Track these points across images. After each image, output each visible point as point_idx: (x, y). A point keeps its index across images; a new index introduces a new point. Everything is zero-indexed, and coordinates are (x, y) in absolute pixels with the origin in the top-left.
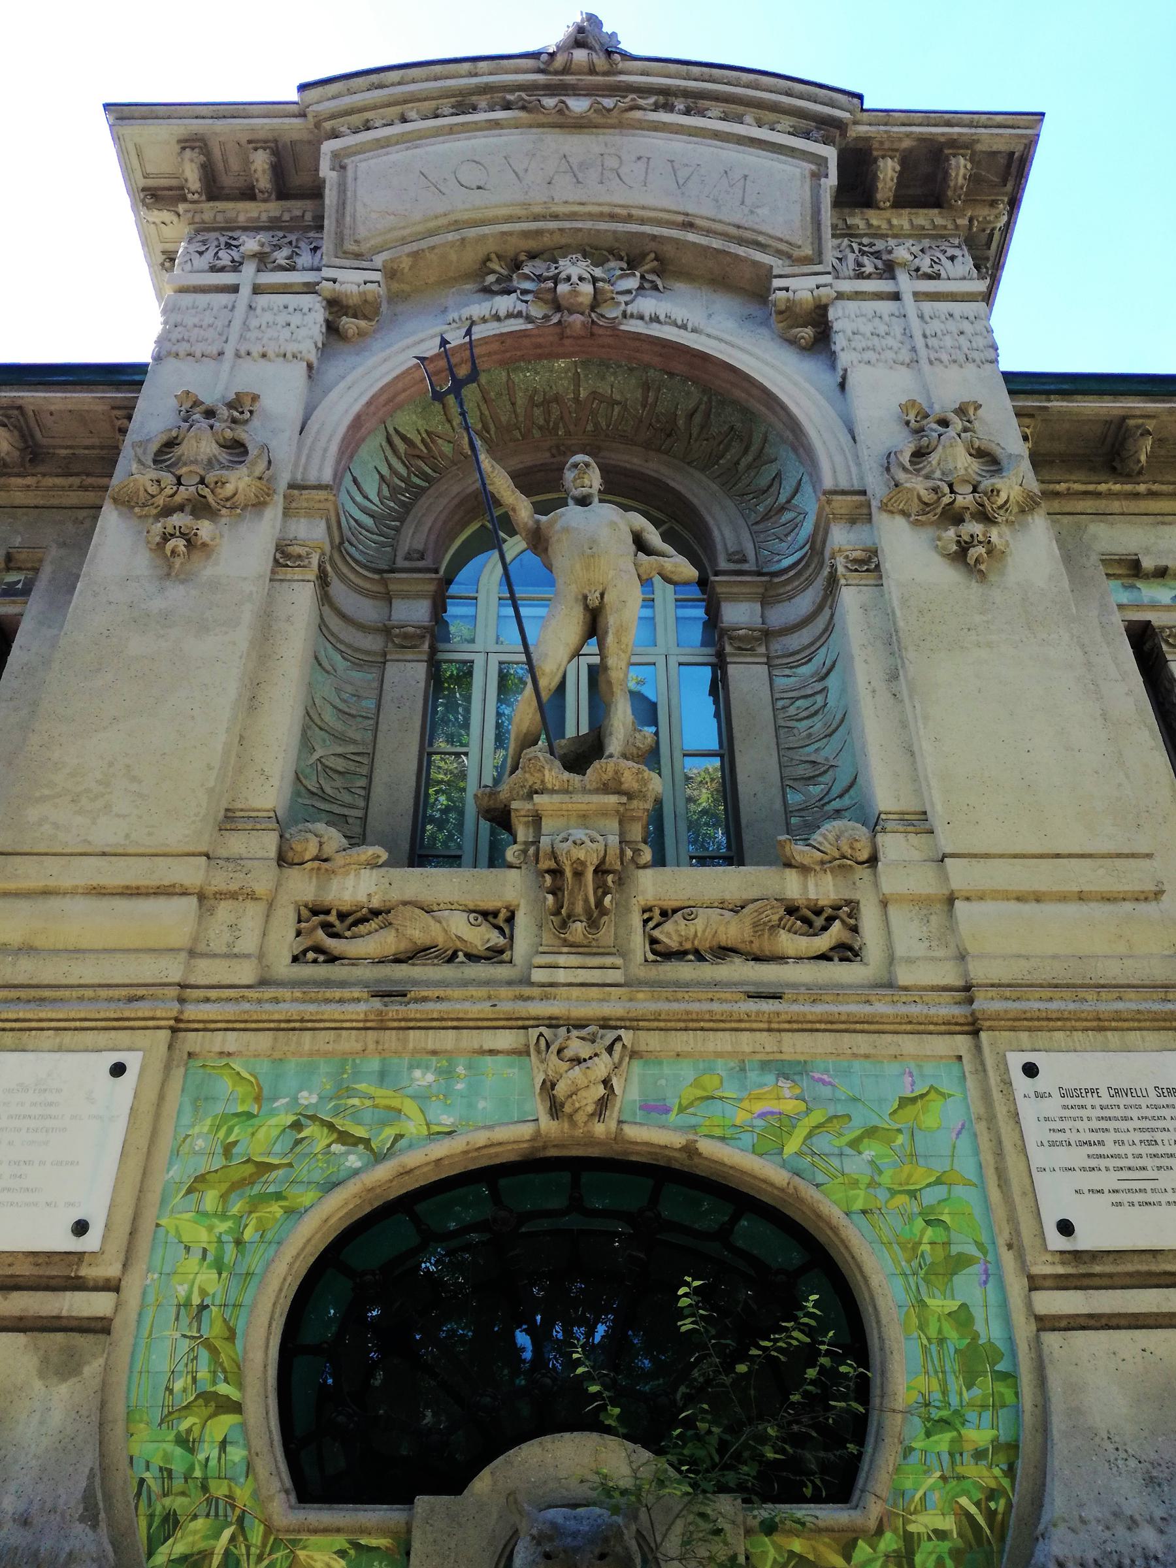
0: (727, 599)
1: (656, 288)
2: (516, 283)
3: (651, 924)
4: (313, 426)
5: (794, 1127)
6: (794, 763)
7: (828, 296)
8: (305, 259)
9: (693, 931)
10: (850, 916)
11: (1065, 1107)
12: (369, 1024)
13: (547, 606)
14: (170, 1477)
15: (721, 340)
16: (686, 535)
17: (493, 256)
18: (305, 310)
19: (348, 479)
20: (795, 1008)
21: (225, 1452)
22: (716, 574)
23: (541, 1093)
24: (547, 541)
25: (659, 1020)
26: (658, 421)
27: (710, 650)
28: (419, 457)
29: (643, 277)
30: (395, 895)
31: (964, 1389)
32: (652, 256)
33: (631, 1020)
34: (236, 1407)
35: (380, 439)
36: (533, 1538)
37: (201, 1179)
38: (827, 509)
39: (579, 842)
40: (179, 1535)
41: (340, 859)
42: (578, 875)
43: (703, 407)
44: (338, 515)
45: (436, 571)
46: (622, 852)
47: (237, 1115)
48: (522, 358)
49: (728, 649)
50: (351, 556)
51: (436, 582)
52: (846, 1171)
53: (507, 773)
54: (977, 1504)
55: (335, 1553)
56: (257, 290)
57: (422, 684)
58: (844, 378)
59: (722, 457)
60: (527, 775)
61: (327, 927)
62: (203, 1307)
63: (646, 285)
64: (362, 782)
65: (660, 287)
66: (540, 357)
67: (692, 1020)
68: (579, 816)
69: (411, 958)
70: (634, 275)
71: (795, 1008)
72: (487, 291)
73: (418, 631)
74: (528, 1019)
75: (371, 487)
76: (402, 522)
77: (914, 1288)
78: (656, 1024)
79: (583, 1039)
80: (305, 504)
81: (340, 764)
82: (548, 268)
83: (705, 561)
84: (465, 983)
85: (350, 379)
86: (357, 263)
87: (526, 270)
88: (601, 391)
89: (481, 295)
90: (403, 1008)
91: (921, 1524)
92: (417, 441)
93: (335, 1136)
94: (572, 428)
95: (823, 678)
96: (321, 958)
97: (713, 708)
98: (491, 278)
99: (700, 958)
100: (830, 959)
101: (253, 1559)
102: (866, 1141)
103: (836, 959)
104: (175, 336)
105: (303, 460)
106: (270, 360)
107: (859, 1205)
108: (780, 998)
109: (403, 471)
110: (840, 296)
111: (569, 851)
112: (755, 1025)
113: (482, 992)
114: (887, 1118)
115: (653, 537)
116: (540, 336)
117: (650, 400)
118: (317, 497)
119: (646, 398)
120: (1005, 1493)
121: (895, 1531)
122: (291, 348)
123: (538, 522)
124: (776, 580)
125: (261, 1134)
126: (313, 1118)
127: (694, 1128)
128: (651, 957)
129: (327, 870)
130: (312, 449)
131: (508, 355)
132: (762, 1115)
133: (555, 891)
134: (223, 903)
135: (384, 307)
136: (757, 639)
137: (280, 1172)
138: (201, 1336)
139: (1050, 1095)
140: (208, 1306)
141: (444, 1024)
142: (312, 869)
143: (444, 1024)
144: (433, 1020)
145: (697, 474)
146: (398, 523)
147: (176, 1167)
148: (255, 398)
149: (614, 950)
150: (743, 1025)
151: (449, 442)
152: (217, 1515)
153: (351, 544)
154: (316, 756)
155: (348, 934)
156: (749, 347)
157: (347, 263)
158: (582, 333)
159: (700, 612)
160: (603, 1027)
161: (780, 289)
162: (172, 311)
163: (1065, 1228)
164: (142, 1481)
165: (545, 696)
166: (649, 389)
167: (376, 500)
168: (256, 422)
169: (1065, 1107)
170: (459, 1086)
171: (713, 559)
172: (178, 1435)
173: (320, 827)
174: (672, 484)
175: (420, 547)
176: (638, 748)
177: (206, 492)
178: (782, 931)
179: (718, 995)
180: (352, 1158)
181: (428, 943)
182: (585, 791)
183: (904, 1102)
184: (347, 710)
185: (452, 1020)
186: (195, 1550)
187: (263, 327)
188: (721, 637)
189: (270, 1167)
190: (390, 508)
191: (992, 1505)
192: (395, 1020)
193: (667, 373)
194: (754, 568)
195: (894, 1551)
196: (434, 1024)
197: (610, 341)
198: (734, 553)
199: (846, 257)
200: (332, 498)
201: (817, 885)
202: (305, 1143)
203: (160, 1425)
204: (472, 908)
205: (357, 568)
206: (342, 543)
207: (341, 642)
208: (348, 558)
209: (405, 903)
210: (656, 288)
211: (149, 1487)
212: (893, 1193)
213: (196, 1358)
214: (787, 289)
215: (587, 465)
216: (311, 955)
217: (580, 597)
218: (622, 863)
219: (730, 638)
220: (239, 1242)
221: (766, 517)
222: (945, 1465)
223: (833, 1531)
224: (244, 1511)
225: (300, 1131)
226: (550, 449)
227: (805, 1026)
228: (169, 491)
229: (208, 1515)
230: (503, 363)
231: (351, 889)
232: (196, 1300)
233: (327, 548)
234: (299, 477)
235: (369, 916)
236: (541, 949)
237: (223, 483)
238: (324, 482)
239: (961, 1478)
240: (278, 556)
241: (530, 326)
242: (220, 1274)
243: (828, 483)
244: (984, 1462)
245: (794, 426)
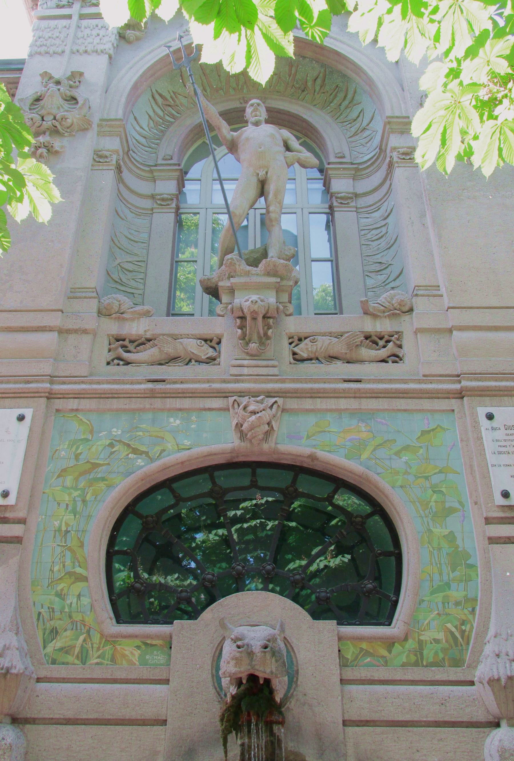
3: (293, 345)
5: (366, 446)
6: (370, 263)
10: (398, 339)
11: (507, 435)
14: (53, 611)
16: (314, 145)
19: (132, 117)
21: (80, 600)
22: (329, 164)
23: (235, 430)
24: (237, 146)
27: (327, 206)
28: (169, 106)
31: (450, 572)
34: (85, 579)
35: (149, 96)
36: (232, 640)
37: (64, 470)
40: (59, 638)
42: (254, 319)
43: (321, 75)
44: (126, 136)
45: (179, 165)
47: (82, 440)
49: (335, 204)
50: (135, 159)
52: (393, 467)
54: (456, 627)
55: (135, 647)
56: (82, 17)
57: (172, 225)
59: (331, 103)
61: (123, 346)
62: (67, 532)
75: (144, 122)
77: (426, 523)
78: (295, 395)
79: (257, 402)
83: (323, 158)
91: (426, 637)
92: (168, 97)
93: (131, 450)
95: (385, 219)
96: (121, 363)
97: (327, 237)
100: (387, 362)
101: (95, 649)
102: (403, 452)
103: (390, 362)
104: (38, 43)
106: (89, 54)
107: (399, 483)
108: (361, 381)
109: (161, 113)
112: (347, 395)
114: (415, 441)
115: (294, 143)
117: (293, 72)
119: (290, 70)
120: (470, 622)
121: (414, 639)
122: (100, 47)
123: (232, 136)
124: (361, 167)
125: (94, 449)
126: (119, 441)
127: (314, 446)
132: (350, 440)
133: (242, 327)
134: (70, 336)
137: (104, 467)
138: (67, 546)
139: (499, 429)
140: (70, 531)
143: (185, 395)
144: (179, 393)
145: (319, 112)
146: (159, 141)
147: (52, 465)
148: (81, 74)
151: (185, 97)
152: (77, 629)
153: (134, 152)
154: (117, 262)
159: (319, 186)
162: (37, 30)
163: (506, 495)
164: (40, 613)
166: (292, 66)
168: (82, 87)
169: (507, 435)
170: (193, 426)
171: (327, 157)
172: (57, 592)
174: (305, 117)
175: (170, 153)
177: (57, 124)
178: (363, 348)
180: (139, 461)
181: (176, 355)
183: (424, 433)
186: (66, 645)
187: (85, 37)
188: (331, 197)
189: (99, 465)
191: (463, 627)
192: (159, 393)
193: (302, 57)
194: (349, 161)
195: (413, 649)
196: (180, 395)
198: (339, 153)
202: (116, 453)
203: (48, 587)
206: (128, 151)
211: (43, 616)
212: (417, 477)
213: (64, 556)
215: (258, 105)
216: (116, 361)
218: (278, 313)
220: (84, 501)
222: (440, 609)
223: (383, 638)
224: (90, 627)
225: (113, 447)
227: (373, 395)
228: (37, 124)
229: (72, 629)
232: (64, 528)
233: (121, 153)
235: (146, 342)
237: (66, 119)
238: (118, 117)
239: (448, 614)
240: (95, 157)
242: (75, 516)
243: (388, 113)
244: (460, 607)
245: (370, 82)
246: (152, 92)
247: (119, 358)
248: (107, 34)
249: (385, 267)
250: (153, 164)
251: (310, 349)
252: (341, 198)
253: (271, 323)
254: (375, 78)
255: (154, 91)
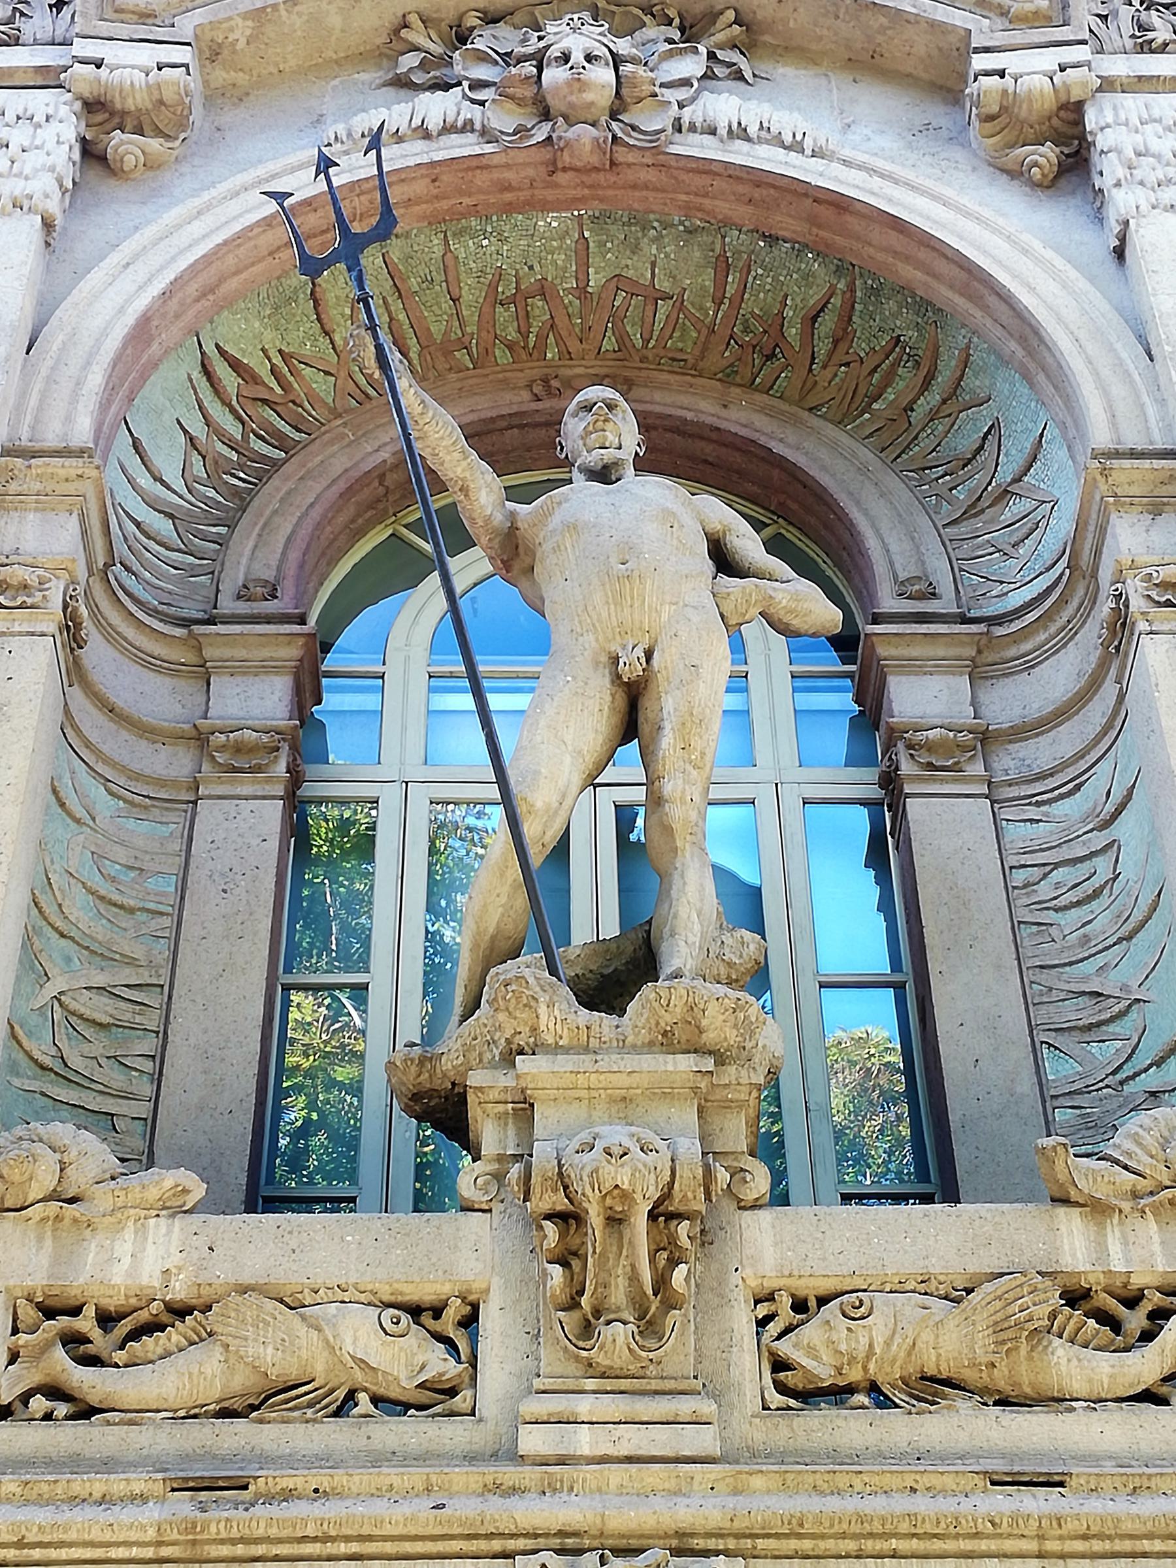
0: (892, 673)
1: (739, 76)
2: (461, 67)
3: (773, 1328)
4: (53, 339)
6: (1054, 995)
7: (1085, 84)
8: (39, 22)
9: (864, 1341)
12: (165, 1552)
13: (532, 690)
15: (872, 171)
17: (413, 19)
18: (39, 118)
19: (123, 440)
20: (1096, 1506)
22: (876, 619)
25: (799, 1536)
26: (746, 330)
27: (871, 774)
28: (265, 401)
29: (711, 56)
30: (222, 1273)
32: (730, 15)
33: (738, 1536)
38: (1103, 487)
39: (617, 1151)
41: (103, 1199)
42: (615, 1221)
43: (836, 301)
45: (302, 620)
46: (708, 1173)
48: (474, 210)
49: (906, 768)
51: (301, 641)
53: (456, 1019)
57: (274, 844)
58: (1123, 239)
60: (502, 1017)
61: (73, 1341)
63: (719, 71)
64: (149, 1045)
65: (748, 75)
66: (509, 209)
67: (871, 1535)
68: (612, 1100)
69: (254, 1408)
70: (696, 51)
71: (1096, 1506)
72: (403, 83)
73: (265, 738)
74: (513, 1536)
76: (231, 527)
78: (793, 1544)
80: (37, 486)
81: (101, 1008)
82: (524, 41)
84: (377, 1460)
85: (129, 247)
86: (142, 31)
87: (480, 44)
88: (630, 273)
89: (390, 92)
90: (240, 1513)
92: (264, 371)
94: (574, 346)
96: (62, 1409)
97: (873, 893)
98: (410, 61)
99: (883, 1401)
105: (33, 401)
108: (1061, 1484)
109: (234, 429)
110: (1107, 85)
111: (597, 1170)
112: (1009, 1545)
113: (415, 1477)
116: (507, 166)
117: (730, 290)
118: (62, 473)
123: (513, 515)
124: (999, 631)
128: (776, 1399)
129: (75, 1221)
130: (50, 380)
131: (445, 204)
135: (197, 115)
136: (963, 748)
141: (330, 1548)
142: (44, 1220)
143: (330, 1548)
144: (304, 1539)
145: (831, 430)
146: (223, 530)
149: (698, 1384)
150: (984, 1545)
151: (327, 373)
154: (51, 990)
155: (119, 1356)
156: (929, 183)
157: (124, 30)
158: (595, 160)
159: (844, 701)
160: (677, 1552)
161: (987, 74)
165: (536, 858)
167: (179, 485)
173: (63, 1131)
174: (778, 448)
175: (269, 575)
176: (730, 964)
178: (1057, 1342)
179: (925, 1480)
181: (294, 1375)
182: (623, 1047)
184: (116, 897)
185: (347, 1539)
188: (888, 747)
190: (206, 500)
192: (222, 1542)
197: (650, 176)
198: (910, 580)
199: (1116, 13)
200: (94, 473)
201: (1125, 1243)
204: (386, 1298)
205: (140, 615)
207: (107, 761)
208: (120, 594)
209: (244, 1290)
210: (739, 76)
214: (1002, 74)
215: (611, 406)
216: (39, 1404)
217: (604, 659)
218: (708, 1198)
219: (910, 746)
221: (972, 510)
226: (529, 386)
227: (1118, 1546)
230: (435, 221)
231: (127, 1261)
233: (82, 573)
234: (25, 433)
235: (165, 1318)
236: (538, 1384)
241: (489, 148)
243: (1101, 436)
246: (203, 353)
247: (55, 1392)
248: (38, 142)
249: (1116, 1009)
250: (200, 615)
251: (843, 1347)
252: (929, 747)
253: (684, 1241)
254: (1041, 314)
255: (210, 349)
